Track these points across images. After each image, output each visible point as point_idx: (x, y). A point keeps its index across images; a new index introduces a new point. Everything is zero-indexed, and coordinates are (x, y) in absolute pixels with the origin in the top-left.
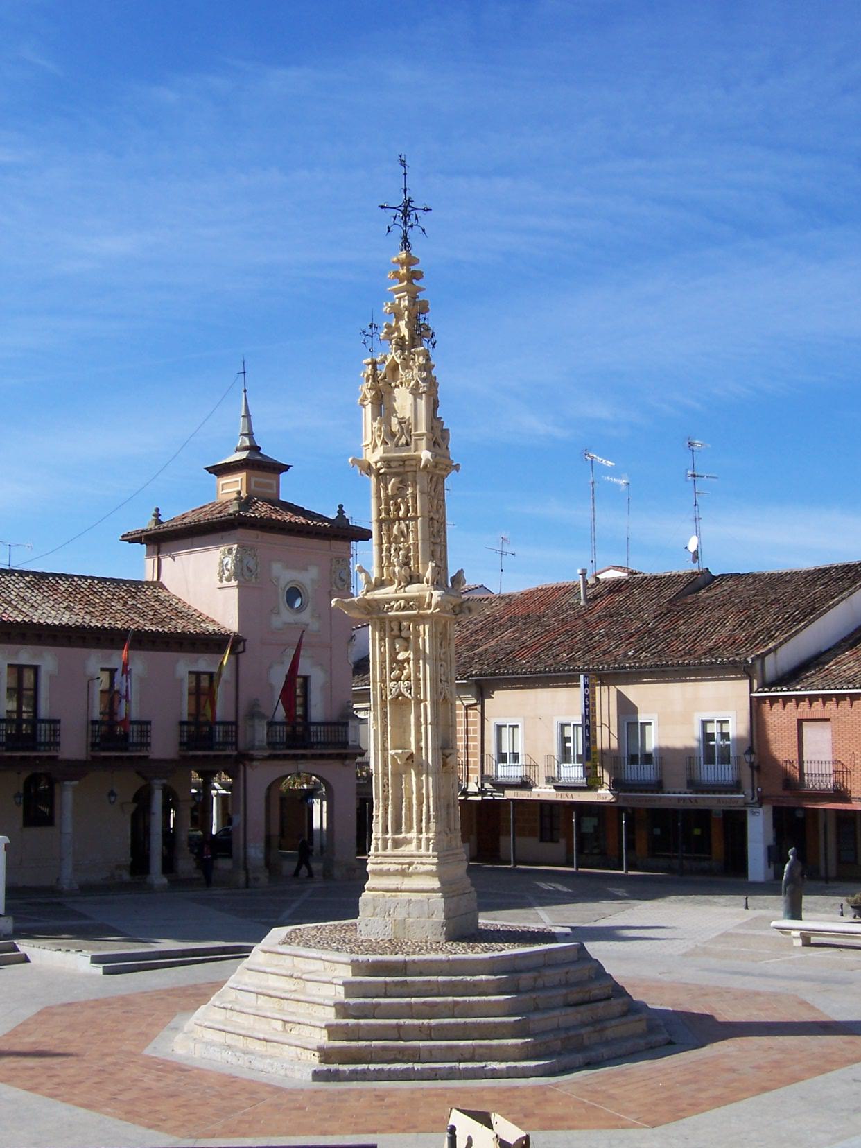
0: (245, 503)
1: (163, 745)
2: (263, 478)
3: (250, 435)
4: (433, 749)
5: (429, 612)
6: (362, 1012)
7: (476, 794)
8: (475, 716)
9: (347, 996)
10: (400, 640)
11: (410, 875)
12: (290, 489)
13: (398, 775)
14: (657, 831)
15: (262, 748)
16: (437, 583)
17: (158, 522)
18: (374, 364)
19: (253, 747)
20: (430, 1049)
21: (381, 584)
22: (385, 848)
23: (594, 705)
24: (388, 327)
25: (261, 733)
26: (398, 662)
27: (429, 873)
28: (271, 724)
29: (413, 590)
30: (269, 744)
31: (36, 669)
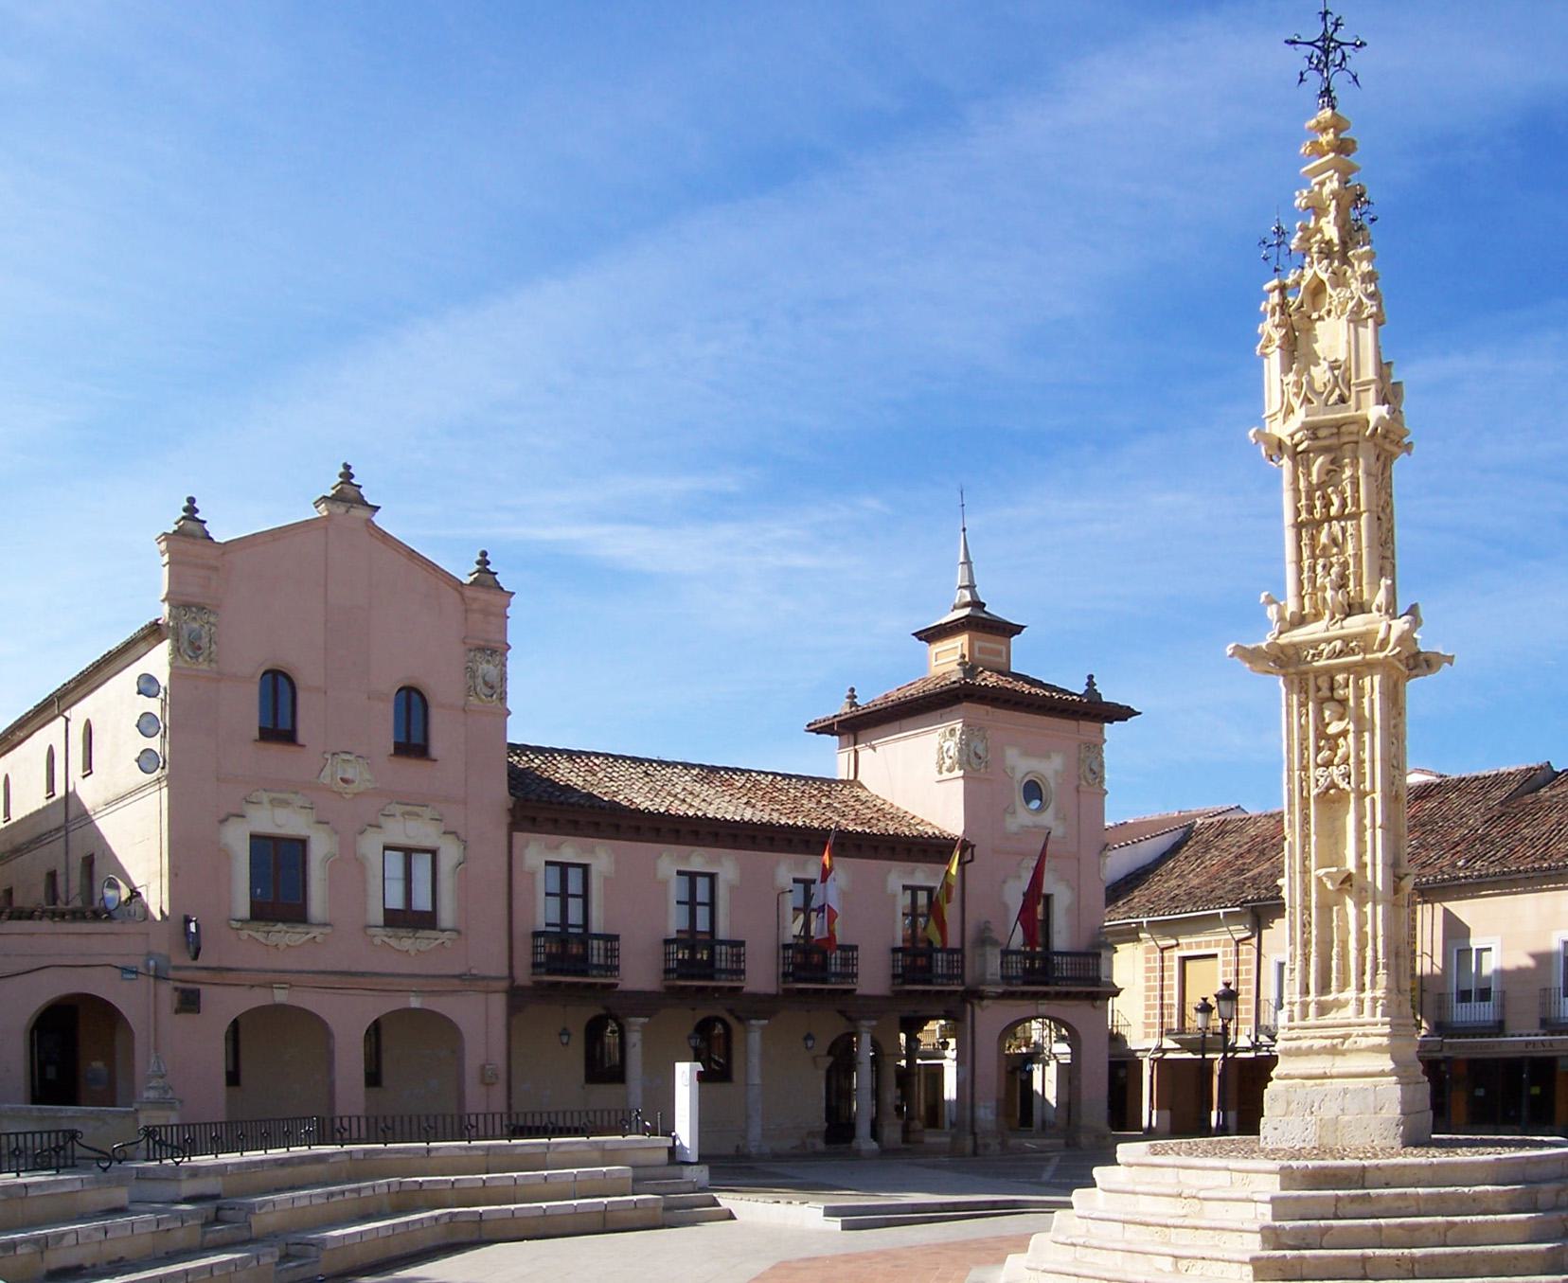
0: (970, 668)
1: (873, 977)
3: (971, 587)
4: (1385, 864)
5: (1381, 655)
6: (1303, 1241)
7: (1248, 1050)
8: (1249, 953)
9: (1275, 1218)
10: (1332, 705)
11: (1343, 1053)
14: (1480, 1092)
15: (995, 983)
16: (1391, 610)
17: (853, 704)
18: (1283, 289)
19: (984, 982)
21: (1300, 620)
22: (1305, 1016)
24: (1304, 229)
25: (994, 964)
26: (1328, 738)
27: (1376, 1049)
28: (1006, 953)
29: (1356, 624)
31: (712, 877)
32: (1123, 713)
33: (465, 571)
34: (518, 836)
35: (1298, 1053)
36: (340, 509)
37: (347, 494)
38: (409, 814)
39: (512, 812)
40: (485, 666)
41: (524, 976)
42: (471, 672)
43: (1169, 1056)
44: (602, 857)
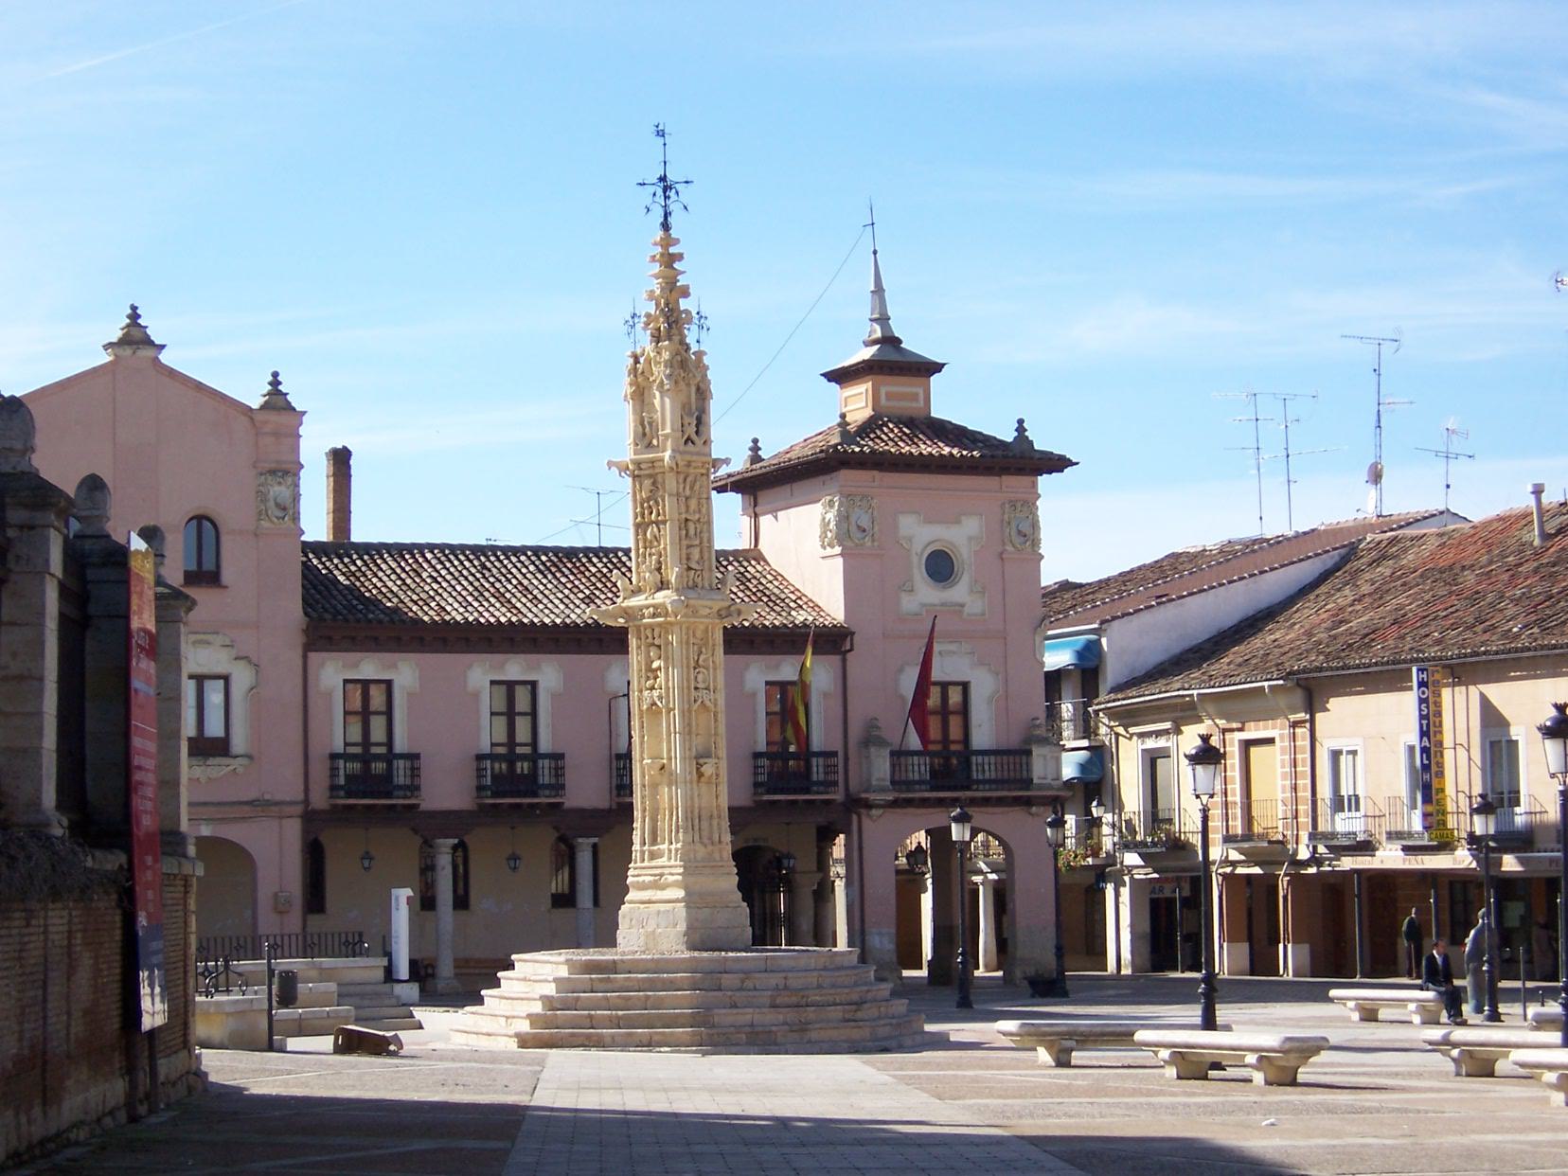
2: (900, 386)
3: (883, 320)
12: (946, 402)
13: (655, 786)
15: (883, 790)
17: (756, 458)
20: (613, 1036)
23: (1439, 714)
25: (881, 767)
27: (675, 884)
28: (899, 755)
30: (893, 782)
32: (1057, 464)
33: (254, 397)
34: (313, 656)
35: (643, 887)
36: (127, 351)
37: (135, 338)
38: (200, 642)
39: (306, 632)
40: (277, 488)
41: (320, 800)
42: (262, 496)
43: (1240, 870)
44: (405, 672)
